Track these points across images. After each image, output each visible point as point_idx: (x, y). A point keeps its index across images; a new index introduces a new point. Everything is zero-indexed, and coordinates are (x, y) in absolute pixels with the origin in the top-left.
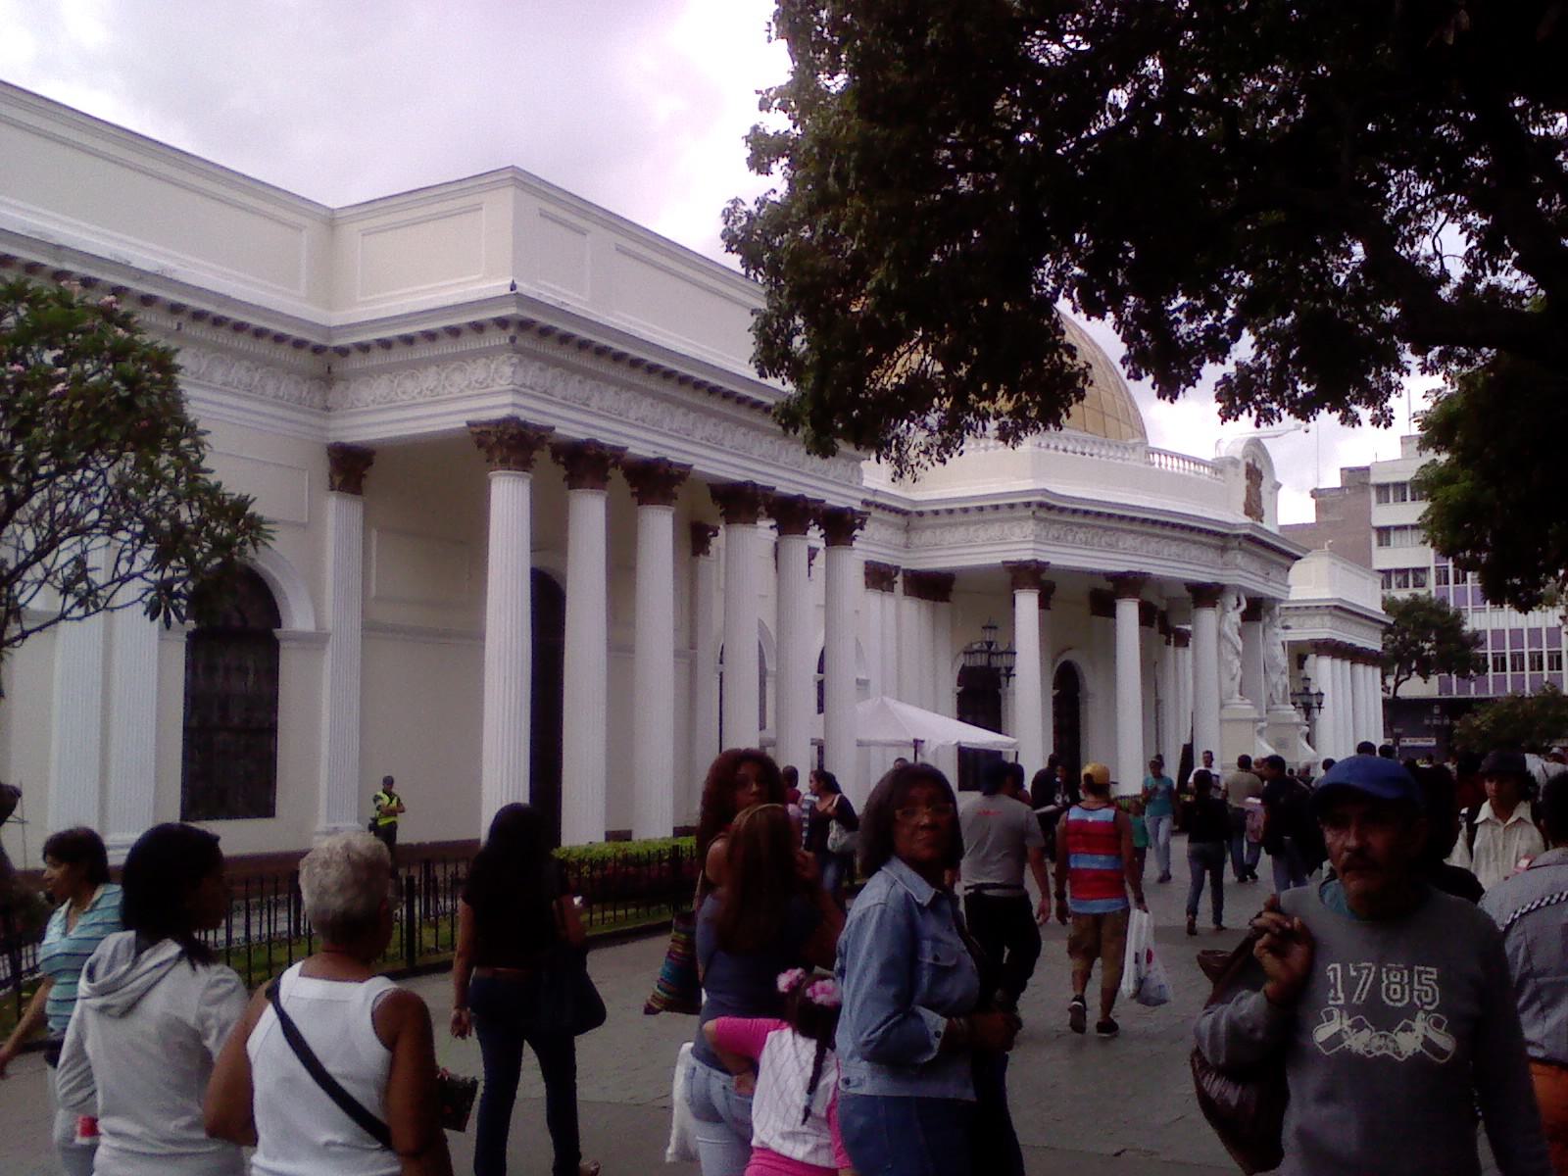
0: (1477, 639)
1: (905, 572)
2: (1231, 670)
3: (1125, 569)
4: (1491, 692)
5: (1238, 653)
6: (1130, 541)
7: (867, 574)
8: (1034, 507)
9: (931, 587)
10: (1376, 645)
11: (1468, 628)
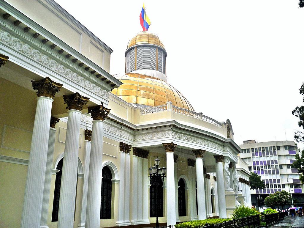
0: (263, 181)
1: (133, 148)
2: (227, 181)
3: (198, 149)
4: (267, 192)
5: (229, 175)
6: (199, 141)
7: (120, 146)
8: (172, 127)
9: (141, 153)
10: (248, 180)
11: (261, 179)
